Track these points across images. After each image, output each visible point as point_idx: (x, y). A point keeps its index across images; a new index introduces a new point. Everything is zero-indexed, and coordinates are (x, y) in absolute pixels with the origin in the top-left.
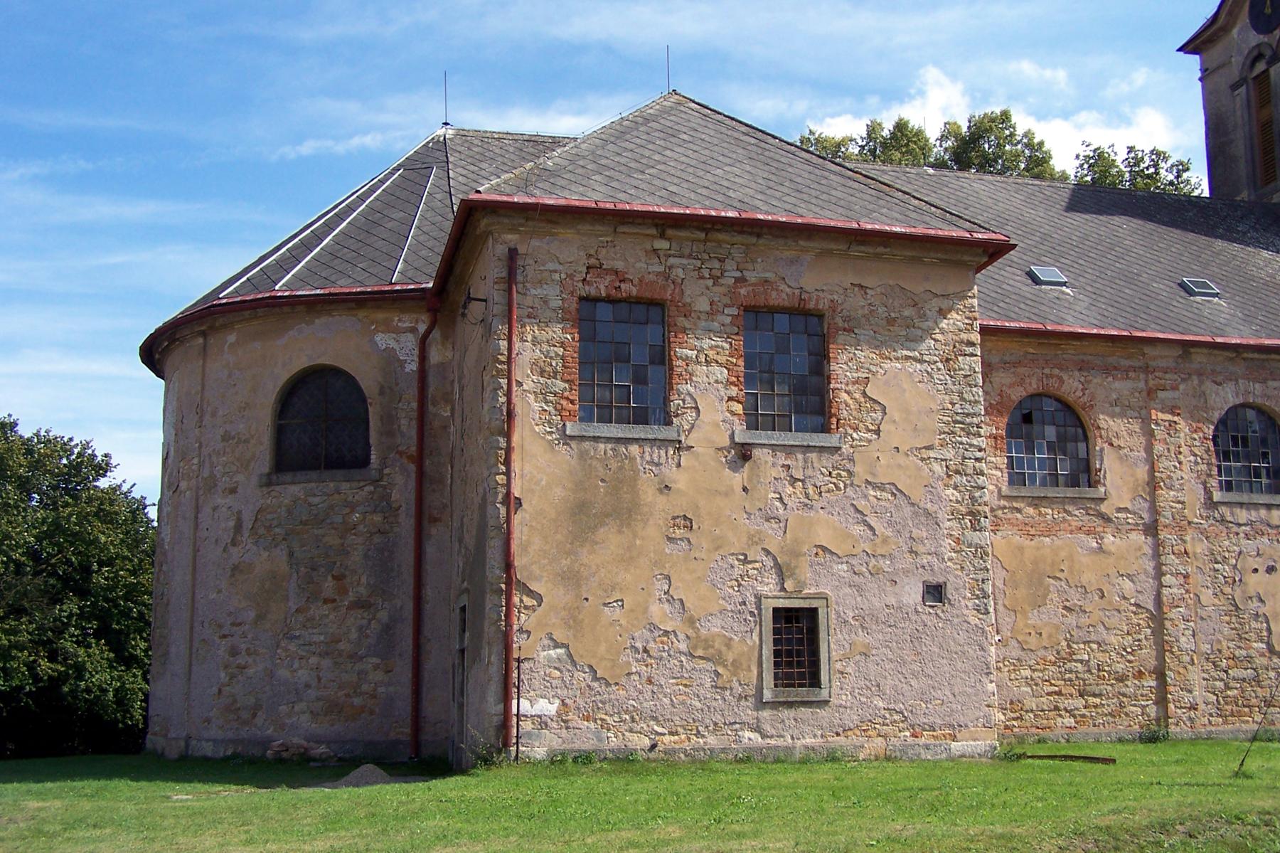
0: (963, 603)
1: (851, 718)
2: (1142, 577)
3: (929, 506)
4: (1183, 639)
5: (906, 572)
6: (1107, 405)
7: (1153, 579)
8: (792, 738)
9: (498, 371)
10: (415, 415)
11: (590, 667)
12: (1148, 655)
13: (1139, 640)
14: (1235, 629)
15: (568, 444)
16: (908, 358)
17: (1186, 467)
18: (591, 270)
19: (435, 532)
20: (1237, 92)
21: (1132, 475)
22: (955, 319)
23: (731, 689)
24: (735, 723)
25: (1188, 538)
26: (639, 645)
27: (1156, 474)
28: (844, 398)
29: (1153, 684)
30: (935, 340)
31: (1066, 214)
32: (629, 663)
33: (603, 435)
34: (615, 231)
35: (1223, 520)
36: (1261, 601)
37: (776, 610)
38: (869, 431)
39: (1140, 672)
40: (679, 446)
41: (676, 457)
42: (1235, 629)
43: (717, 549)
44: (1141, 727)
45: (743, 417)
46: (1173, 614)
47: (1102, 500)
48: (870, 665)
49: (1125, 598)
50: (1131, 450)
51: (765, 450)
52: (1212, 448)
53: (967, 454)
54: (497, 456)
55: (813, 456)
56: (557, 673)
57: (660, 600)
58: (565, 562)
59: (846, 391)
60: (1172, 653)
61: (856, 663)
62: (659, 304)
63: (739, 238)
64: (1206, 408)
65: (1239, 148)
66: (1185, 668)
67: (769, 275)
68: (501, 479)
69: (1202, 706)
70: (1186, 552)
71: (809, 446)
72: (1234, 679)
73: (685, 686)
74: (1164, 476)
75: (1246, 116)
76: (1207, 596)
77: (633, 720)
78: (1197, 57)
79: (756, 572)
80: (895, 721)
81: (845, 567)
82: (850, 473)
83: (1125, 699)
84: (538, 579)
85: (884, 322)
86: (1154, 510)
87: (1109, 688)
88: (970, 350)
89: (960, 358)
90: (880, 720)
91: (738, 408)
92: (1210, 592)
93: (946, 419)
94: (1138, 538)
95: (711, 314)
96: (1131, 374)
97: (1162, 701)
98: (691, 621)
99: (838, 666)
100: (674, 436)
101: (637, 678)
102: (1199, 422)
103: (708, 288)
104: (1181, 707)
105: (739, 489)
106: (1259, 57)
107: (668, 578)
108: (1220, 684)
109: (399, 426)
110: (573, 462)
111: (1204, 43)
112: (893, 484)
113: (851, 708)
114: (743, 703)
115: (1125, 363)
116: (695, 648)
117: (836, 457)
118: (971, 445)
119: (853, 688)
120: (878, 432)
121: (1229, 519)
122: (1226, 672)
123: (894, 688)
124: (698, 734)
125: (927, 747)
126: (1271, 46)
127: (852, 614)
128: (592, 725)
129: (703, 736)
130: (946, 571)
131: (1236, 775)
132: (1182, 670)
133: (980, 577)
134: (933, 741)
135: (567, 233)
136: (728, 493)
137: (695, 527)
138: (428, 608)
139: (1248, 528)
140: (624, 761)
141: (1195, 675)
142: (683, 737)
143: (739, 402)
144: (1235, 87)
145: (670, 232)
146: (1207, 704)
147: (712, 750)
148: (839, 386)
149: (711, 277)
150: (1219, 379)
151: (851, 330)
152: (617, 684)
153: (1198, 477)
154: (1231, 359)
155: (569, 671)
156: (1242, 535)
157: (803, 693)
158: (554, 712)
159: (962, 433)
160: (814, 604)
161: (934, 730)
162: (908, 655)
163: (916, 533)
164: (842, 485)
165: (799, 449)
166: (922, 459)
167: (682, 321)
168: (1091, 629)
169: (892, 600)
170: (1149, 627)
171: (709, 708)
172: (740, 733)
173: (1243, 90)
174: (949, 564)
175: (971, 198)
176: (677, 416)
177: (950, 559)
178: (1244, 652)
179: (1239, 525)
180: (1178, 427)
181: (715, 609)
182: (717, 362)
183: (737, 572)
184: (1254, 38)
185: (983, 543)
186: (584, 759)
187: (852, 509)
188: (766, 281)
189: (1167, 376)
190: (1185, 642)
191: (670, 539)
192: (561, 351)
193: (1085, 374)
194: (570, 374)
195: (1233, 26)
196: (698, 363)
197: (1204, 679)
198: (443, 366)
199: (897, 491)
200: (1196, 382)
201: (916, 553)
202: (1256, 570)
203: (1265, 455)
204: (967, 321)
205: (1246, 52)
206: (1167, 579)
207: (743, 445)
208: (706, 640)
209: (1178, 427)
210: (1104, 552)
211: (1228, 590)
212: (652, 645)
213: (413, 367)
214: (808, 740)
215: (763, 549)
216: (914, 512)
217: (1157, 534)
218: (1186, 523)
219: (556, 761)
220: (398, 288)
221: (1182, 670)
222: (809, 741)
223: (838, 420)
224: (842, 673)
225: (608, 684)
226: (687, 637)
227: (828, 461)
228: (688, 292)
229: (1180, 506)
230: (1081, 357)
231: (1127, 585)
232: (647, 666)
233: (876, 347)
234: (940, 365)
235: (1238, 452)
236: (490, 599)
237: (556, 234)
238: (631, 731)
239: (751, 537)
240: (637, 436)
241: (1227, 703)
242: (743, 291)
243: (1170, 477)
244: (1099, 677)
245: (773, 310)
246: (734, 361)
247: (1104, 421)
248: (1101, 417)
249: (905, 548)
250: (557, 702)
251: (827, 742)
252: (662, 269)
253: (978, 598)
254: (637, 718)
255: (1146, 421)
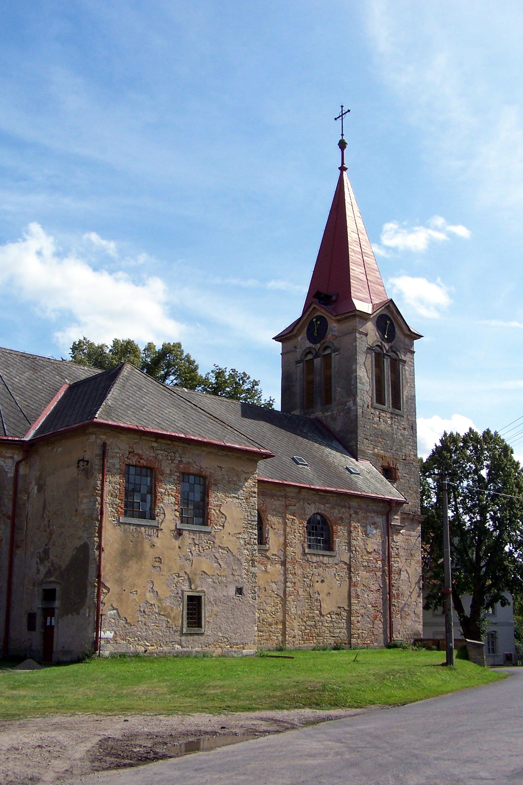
0: (248, 595)
1: (211, 640)
2: (280, 583)
3: (239, 556)
4: (292, 609)
5: (230, 582)
6: (271, 511)
7: (283, 584)
8: (192, 648)
9: (97, 494)
10: (11, 497)
11: (125, 618)
12: (280, 614)
13: (277, 609)
14: (310, 605)
15: (119, 526)
16: (234, 497)
17: (297, 538)
18: (131, 454)
19: (19, 552)
20: (298, 365)
21: (279, 541)
22: (250, 483)
23: (172, 628)
24: (173, 642)
25: (296, 567)
26: (142, 610)
27: (287, 541)
28: (213, 512)
29: (281, 627)
30: (243, 490)
31: (242, 418)
32: (138, 617)
33: (132, 523)
34: (140, 438)
35: (308, 561)
36: (319, 594)
37: (188, 596)
38: (221, 526)
39: (277, 622)
40: (158, 529)
41: (157, 533)
42: (310, 605)
43: (170, 571)
44: (276, 645)
45: (179, 518)
46: (289, 599)
47: (267, 550)
48: (218, 619)
49: (273, 592)
50: (278, 530)
51: (187, 532)
52: (306, 531)
53: (252, 537)
54: (95, 529)
55: (202, 535)
56: (113, 621)
57: (150, 591)
58: (118, 575)
59: (214, 510)
60: (288, 614)
61: (213, 618)
62: (151, 469)
63: (182, 445)
64: (305, 514)
65: (298, 388)
66: (292, 621)
67: (190, 460)
68: (96, 539)
69: (297, 637)
70: (295, 574)
71: (201, 531)
72: (308, 625)
73: (157, 626)
74: (289, 541)
75: (302, 376)
76: (301, 591)
77: (139, 640)
78: (281, 343)
79: (182, 581)
80: (225, 642)
81: (211, 580)
82: (214, 542)
83: (271, 633)
84: (108, 581)
85: (227, 482)
86: (285, 556)
87: (266, 629)
88: (254, 495)
89: (251, 498)
90: (220, 641)
91: (178, 514)
92: (302, 590)
93: (246, 522)
94: (279, 566)
95: (171, 474)
96: (280, 498)
97: (284, 634)
98: (160, 600)
99: (207, 619)
100: (156, 524)
101: (140, 623)
102: (302, 520)
103: (169, 464)
104: (290, 637)
105: (177, 547)
106: (310, 352)
107: (152, 582)
108: (303, 628)
109: (4, 502)
110: (122, 533)
111: (285, 339)
112: (227, 547)
113: (211, 636)
114: (176, 633)
115: (279, 493)
116: (161, 611)
117: (210, 536)
118: (253, 533)
119: (212, 628)
120: (223, 526)
121: (310, 560)
122: (306, 623)
123: (225, 628)
124: (161, 646)
125: (235, 652)
126: (315, 349)
127: (212, 599)
128: (124, 642)
129: (162, 647)
130: (244, 582)
131: (354, 661)
132: (291, 622)
133: (254, 585)
134: (237, 650)
135: (123, 437)
136: (174, 549)
137: (162, 562)
138: (14, 587)
139: (316, 564)
140: (137, 656)
141: (295, 624)
142: (155, 647)
143: (178, 512)
144: (298, 362)
145: (159, 440)
146: (299, 635)
147: (165, 653)
148: (211, 507)
149: (171, 459)
150: (310, 502)
151: (216, 485)
152: (134, 625)
153: (300, 543)
154: (314, 494)
155: (118, 620)
156: (314, 567)
157: (196, 630)
158: (112, 637)
159: (250, 528)
160: (201, 594)
161: (237, 645)
162: (230, 616)
163: (235, 567)
164: (211, 547)
165: (197, 532)
166: (237, 538)
167: (160, 477)
168: (261, 604)
169: (225, 594)
170: (281, 603)
171: (164, 635)
172: (174, 646)
173: (301, 364)
174: (244, 580)
175: (205, 407)
176: (157, 516)
177: (245, 578)
178: (312, 615)
179: (313, 563)
180: (295, 521)
181: (168, 596)
182: (172, 495)
183: (176, 581)
184: (308, 344)
185: (255, 572)
186: (123, 656)
187: (214, 557)
188: (189, 463)
189: (293, 500)
190: (293, 610)
191: (154, 567)
192: (119, 487)
193: (264, 497)
194: (122, 496)
195: (299, 335)
196: (165, 495)
197: (298, 625)
198: (25, 476)
199: (229, 550)
200: (302, 503)
201: (234, 575)
202: (318, 581)
203: (322, 534)
204: (254, 483)
205: (304, 349)
206: (288, 584)
207: (180, 529)
208: (165, 608)
209: (295, 521)
210: (267, 572)
211: (308, 589)
212: (146, 610)
213: (11, 475)
214: (197, 649)
215: (185, 572)
216: (234, 559)
217: (286, 565)
218: (295, 561)
219: (113, 656)
220: (10, 438)
221: (291, 622)
222: (197, 649)
223: (211, 521)
224: (208, 622)
225: (131, 625)
226: (158, 606)
227: (204, 537)
228: (163, 465)
229: (294, 554)
230: (263, 490)
231: (274, 586)
232: (144, 618)
233: (224, 492)
234: (244, 500)
235: (313, 532)
236: (89, 590)
237: (120, 437)
238: (138, 644)
239: (181, 567)
240: (144, 524)
241: (305, 635)
242: (181, 466)
243: (291, 542)
244: (263, 624)
245: (189, 474)
246: (177, 494)
247: (270, 517)
248: (269, 516)
249: (230, 573)
250: (113, 633)
251: (203, 649)
252: (154, 455)
253: (253, 593)
254: (140, 639)
255: (284, 518)
